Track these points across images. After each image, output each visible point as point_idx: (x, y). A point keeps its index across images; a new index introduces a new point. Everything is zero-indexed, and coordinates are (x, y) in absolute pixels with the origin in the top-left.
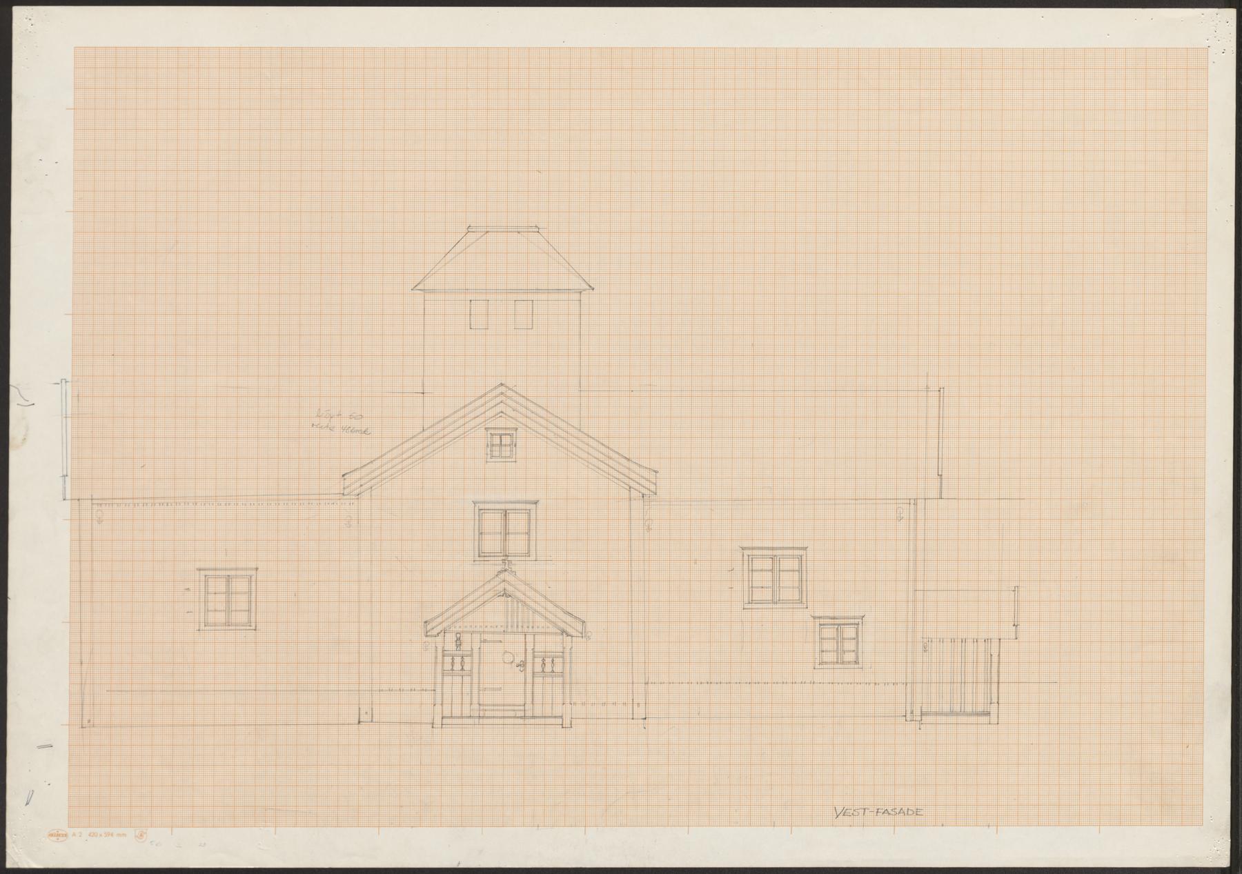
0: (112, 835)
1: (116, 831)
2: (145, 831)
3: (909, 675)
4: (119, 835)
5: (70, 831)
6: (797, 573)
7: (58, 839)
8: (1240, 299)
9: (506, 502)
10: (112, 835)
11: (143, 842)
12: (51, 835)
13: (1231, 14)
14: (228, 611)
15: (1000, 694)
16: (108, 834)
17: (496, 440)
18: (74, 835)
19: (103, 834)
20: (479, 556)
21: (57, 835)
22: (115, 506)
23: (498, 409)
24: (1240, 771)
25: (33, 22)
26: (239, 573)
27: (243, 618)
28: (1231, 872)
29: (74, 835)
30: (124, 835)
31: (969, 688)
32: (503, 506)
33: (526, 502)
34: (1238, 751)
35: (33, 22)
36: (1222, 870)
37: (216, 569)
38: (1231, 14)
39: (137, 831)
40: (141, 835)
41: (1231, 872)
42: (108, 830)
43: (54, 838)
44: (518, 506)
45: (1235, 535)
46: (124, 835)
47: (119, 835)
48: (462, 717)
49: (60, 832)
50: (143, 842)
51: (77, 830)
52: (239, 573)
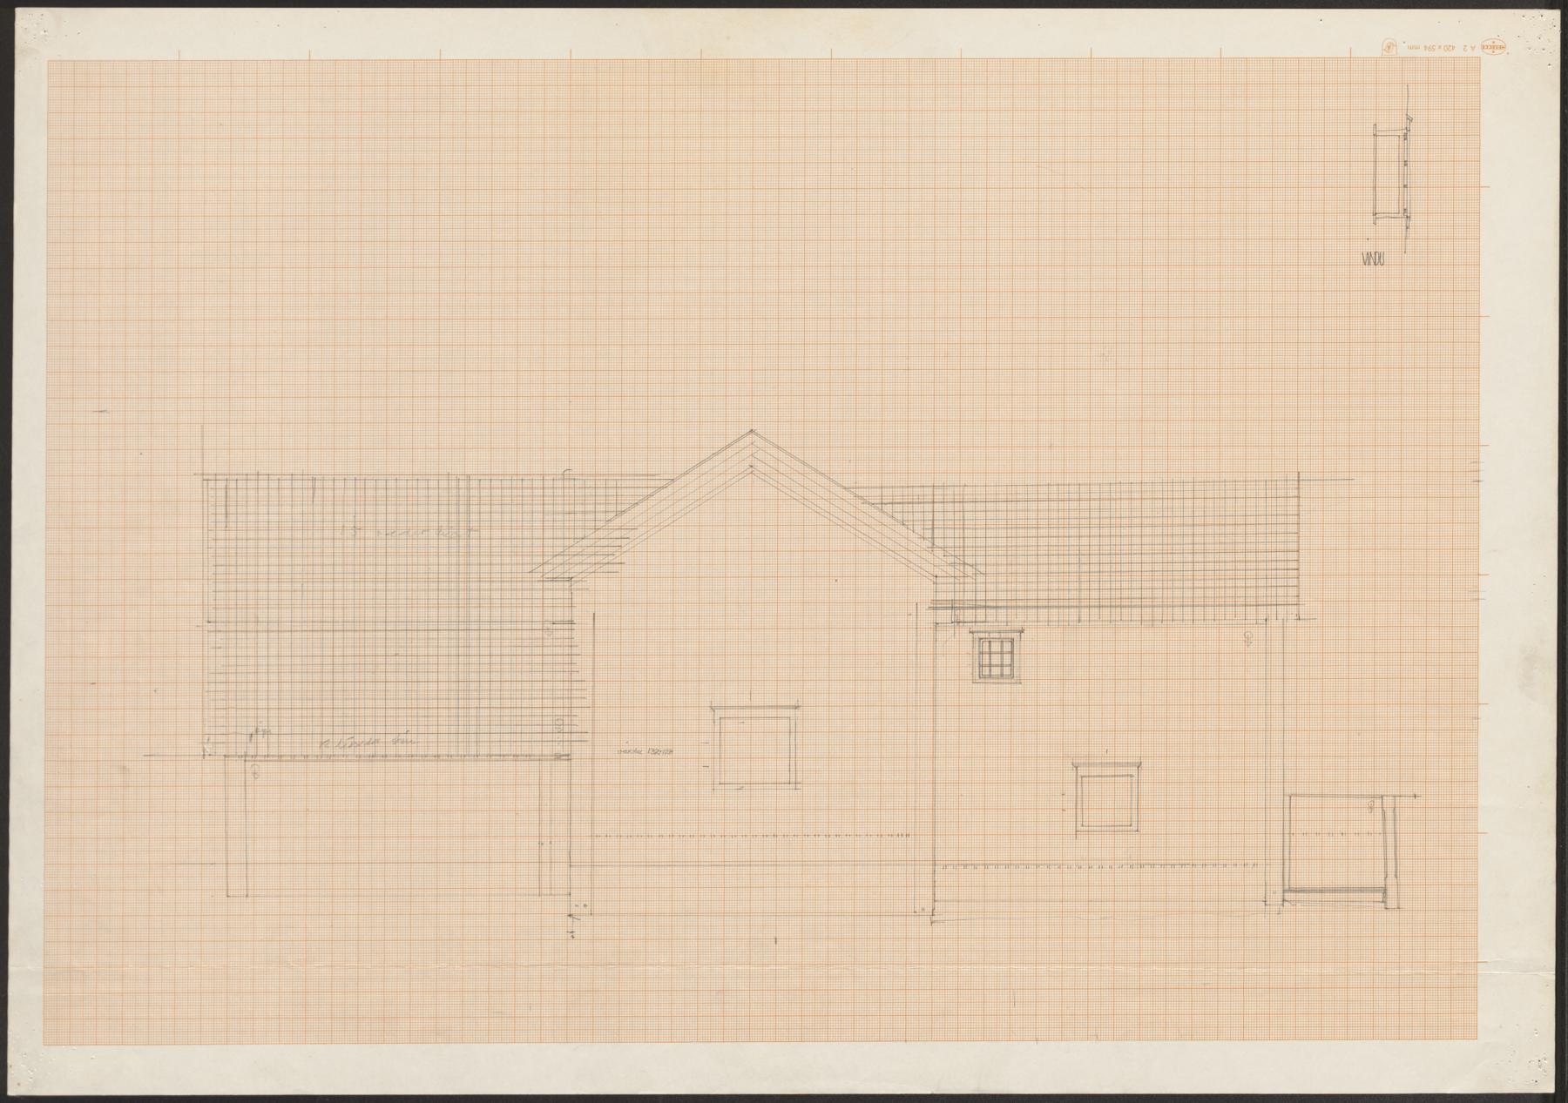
0: (1425, 47)
2: (1384, 53)
3: (793, 775)
4: (1417, 48)
5: (1478, 52)
10: (1425, 47)
11: (1384, 41)
12: (1501, 47)
13: (1555, 15)
15: (1327, 883)
16: (1431, 48)
18: (1473, 48)
20: (1083, 826)
21: (1495, 47)
24: (1566, 981)
28: (1554, 1101)
30: (1410, 48)
37: (1386, 859)
38: (1555, 15)
39: (1394, 52)
40: (1389, 47)
43: (1498, 43)
47: (1417, 48)
49: (1490, 51)
50: (1384, 41)
51: (1469, 53)
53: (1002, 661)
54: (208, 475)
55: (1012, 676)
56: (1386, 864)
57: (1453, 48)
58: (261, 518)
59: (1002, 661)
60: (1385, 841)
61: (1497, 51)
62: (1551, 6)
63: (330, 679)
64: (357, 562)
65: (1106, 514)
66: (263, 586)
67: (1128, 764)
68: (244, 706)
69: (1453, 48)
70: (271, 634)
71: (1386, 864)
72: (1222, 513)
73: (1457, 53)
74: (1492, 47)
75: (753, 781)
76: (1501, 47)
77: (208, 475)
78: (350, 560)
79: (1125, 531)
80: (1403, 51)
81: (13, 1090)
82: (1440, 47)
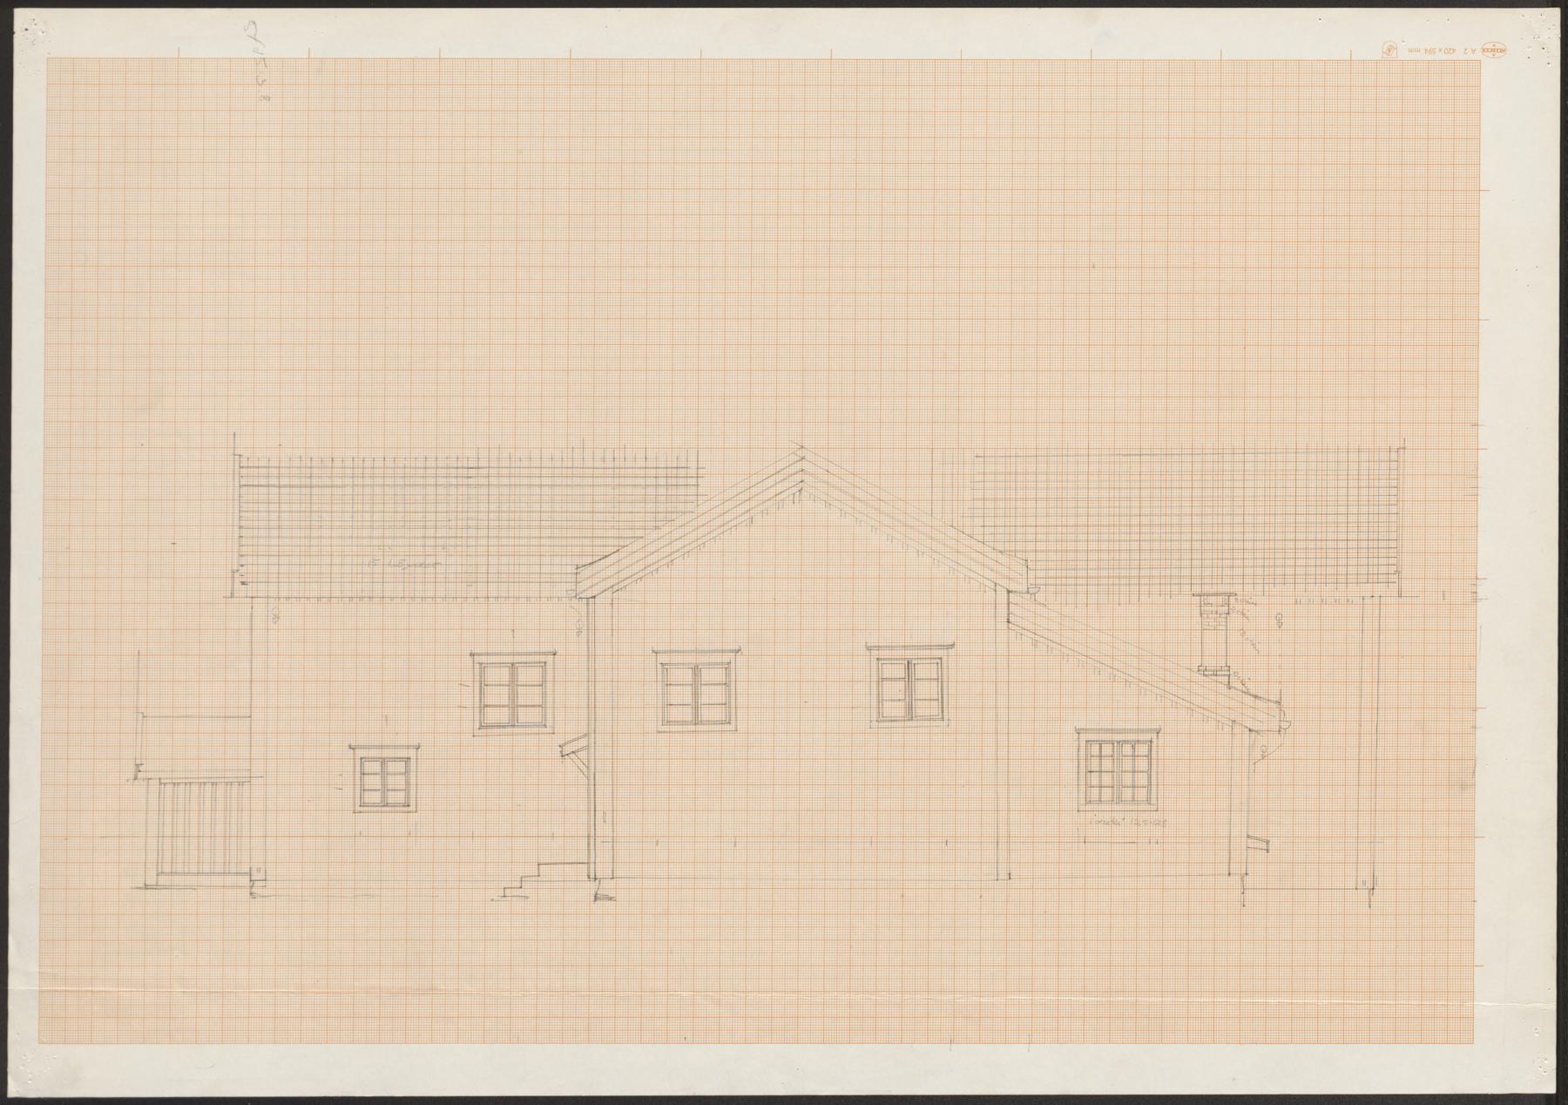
2: (1385, 56)
4: (1418, 51)
5: (1478, 55)
6: (935, 683)
9: (513, 654)
11: (1384, 44)
12: (1502, 51)
13: (1555, 13)
16: (1432, 51)
17: (1095, 750)
18: (1473, 51)
19: (1437, 50)
21: (1497, 50)
25: (36, 22)
28: (1557, 1100)
29: (1473, 51)
30: (1410, 51)
32: (509, 659)
33: (540, 654)
35: (36, 22)
36: (1547, 1097)
40: (1389, 51)
41: (1557, 1100)
42: (1430, 57)
43: (1498, 46)
44: (531, 659)
46: (1410, 51)
47: (1418, 51)
49: (1490, 54)
50: (1384, 44)
51: (1471, 56)
53: (1100, 777)
55: (1149, 801)
59: (1100, 777)
60: (401, 747)
61: (1497, 55)
62: (1554, 6)
63: (334, 568)
64: (1371, 511)
65: (1259, 555)
67: (408, 747)
70: (432, 595)
71: (375, 747)
73: (1459, 55)
74: (1492, 50)
76: (1502, 51)
78: (1364, 509)
80: (1404, 54)
81: (1553, 15)
82: (1440, 50)
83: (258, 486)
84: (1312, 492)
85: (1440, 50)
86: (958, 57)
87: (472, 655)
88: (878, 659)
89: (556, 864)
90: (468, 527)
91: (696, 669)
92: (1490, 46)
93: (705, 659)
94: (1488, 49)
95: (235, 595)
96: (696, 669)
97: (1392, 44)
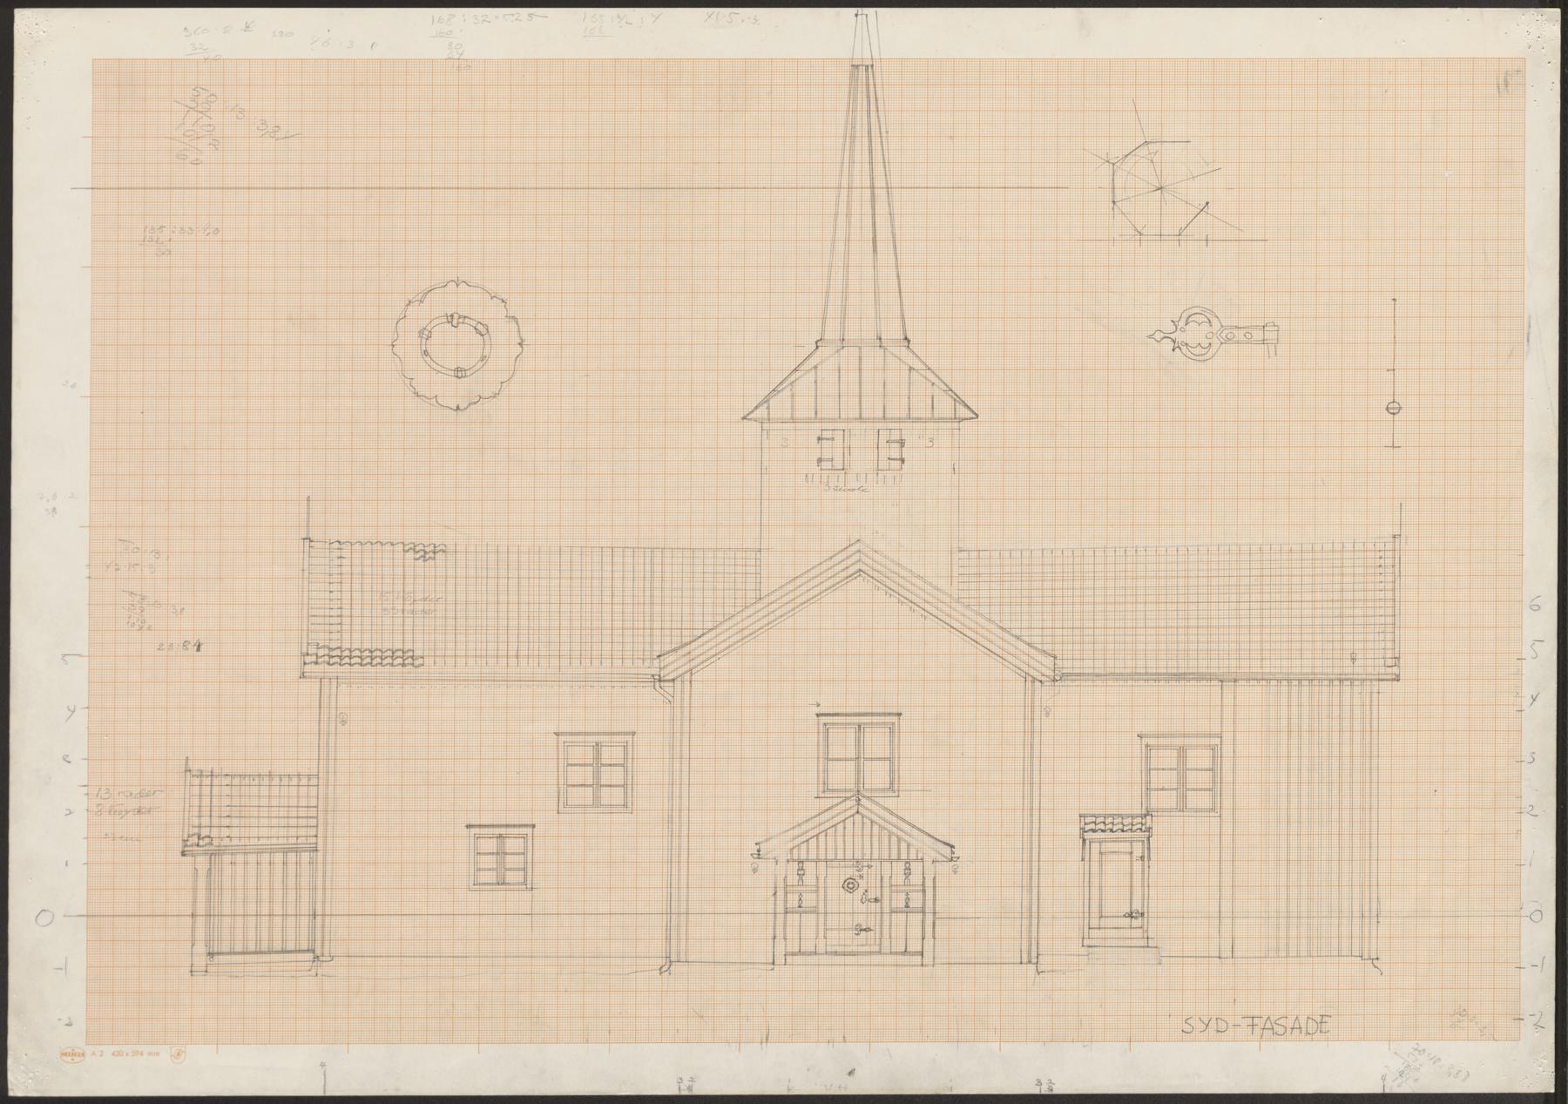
0: (142, 1054)
1: (146, 1049)
4: (150, 1054)
5: (89, 1050)
7: (73, 1060)
8: (1566, 326)
10: (142, 1054)
14: (501, 853)
16: (136, 1053)
18: (94, 1054)
21: (71, 1054)
22: (135, 790)
23: (856, 567)
26: (1162, 741)
27: (1204, 800)
29: (94, 1054)
30: (157, 1054)
31: (278, 921)
34: (1565, 916)
39: (174, 1049)
40: (178, 1054)
45: (1560, 658)
47: (150, 1054)
48: (270, 952)
49: (76, 1050)
52: (1162, 741)
54: (195, 902)
56: (825, 896)
57: (113, 1054)
58: (1243, 646)
61: (69, 1050)
62: (1552, 6)
66: (1203, 646)
68: (1278, 599)
69: (113, 1054)
71: (825, 896)
72: (484, 653)
75: (693, 736)
77: (195, 902)
79: (1370, 595)
83: (1131, 887)
84: (1318, 645)
85: (127, 1054)
86: (613, 1046)
87: (557, 734)
88: (557, 734)
89: (321, 690)
90: (692, 604)
91: (1182, 751)
92: (77, 1059)
93: (1188, 741)
94: (79, 1056)
95: (1175, 753)
96: (1182, 751)
97: (175, 1060)
